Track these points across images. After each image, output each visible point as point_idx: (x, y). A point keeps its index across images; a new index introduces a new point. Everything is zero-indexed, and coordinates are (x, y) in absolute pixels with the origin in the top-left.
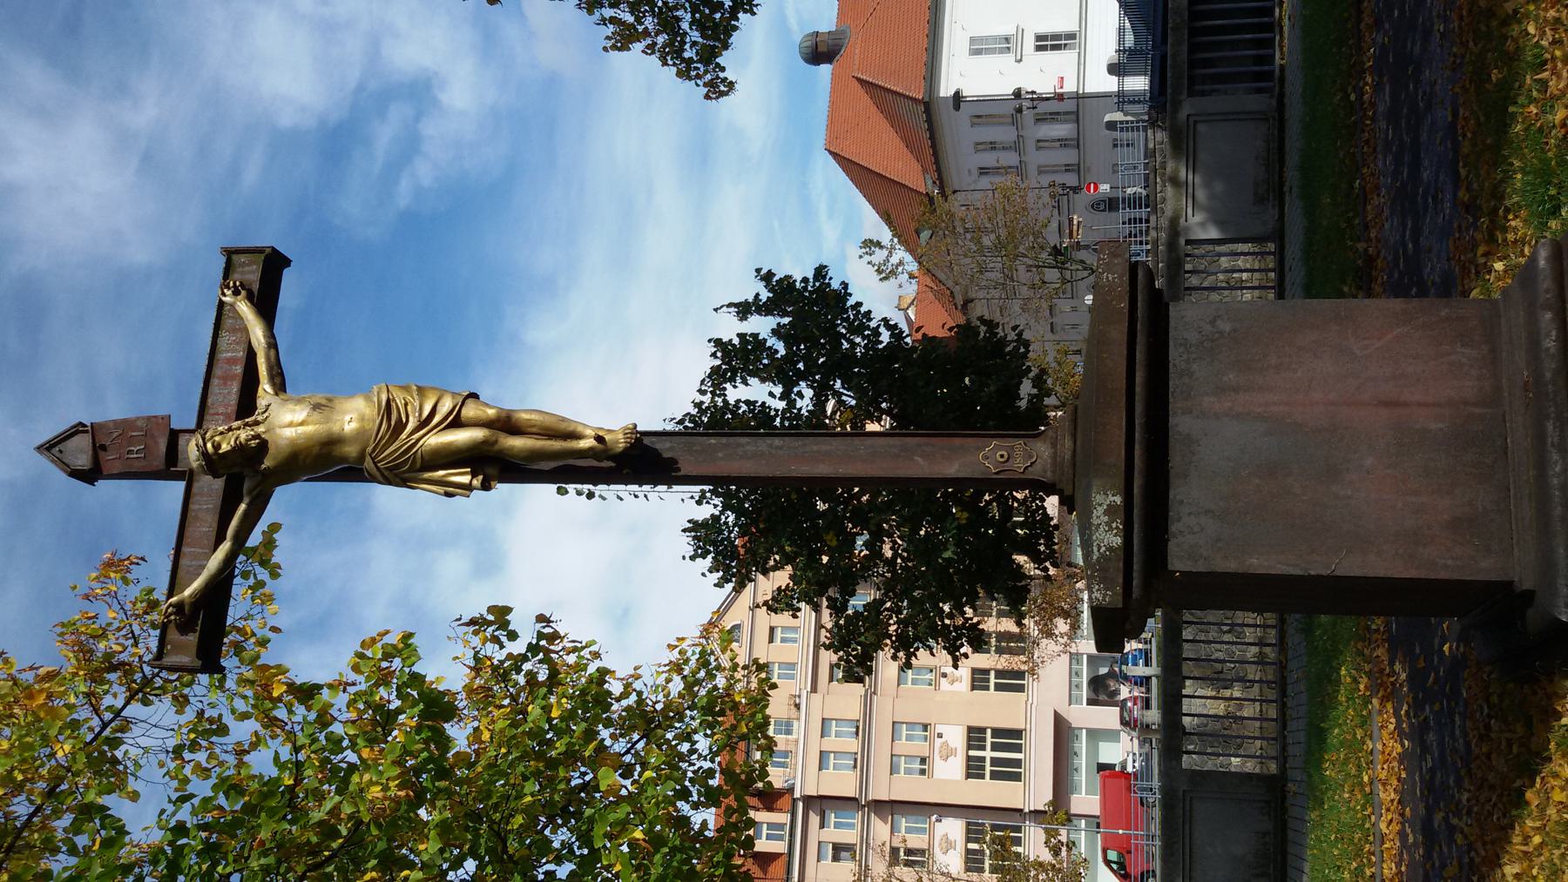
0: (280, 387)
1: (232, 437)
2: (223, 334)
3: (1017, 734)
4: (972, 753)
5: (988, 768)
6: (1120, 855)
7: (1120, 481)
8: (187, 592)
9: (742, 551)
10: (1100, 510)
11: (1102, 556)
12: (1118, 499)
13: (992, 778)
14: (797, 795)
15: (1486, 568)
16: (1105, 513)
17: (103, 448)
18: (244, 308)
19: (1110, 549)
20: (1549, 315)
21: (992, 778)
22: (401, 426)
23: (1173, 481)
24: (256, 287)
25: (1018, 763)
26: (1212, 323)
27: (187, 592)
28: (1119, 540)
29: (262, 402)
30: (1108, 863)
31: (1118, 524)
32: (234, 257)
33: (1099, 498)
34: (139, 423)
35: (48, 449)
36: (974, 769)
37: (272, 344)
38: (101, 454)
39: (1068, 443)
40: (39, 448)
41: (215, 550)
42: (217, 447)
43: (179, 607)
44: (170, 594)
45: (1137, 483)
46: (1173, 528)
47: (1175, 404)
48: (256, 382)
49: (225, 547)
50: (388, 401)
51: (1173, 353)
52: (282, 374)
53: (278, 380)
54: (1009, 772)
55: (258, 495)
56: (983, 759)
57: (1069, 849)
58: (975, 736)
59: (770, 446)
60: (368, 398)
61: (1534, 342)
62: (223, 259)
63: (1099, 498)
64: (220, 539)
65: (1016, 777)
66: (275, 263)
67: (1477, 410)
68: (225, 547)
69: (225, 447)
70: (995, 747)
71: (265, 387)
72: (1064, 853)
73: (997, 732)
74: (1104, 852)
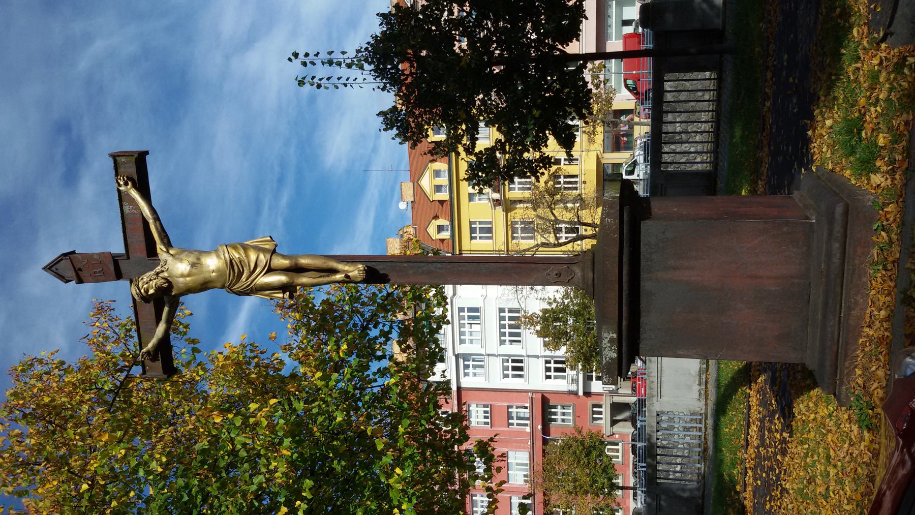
0: (168, 245)
1: (153, 283)
2: (125, 204)
6: (634, 82)
7: (616, 327)
8: (150, 345)
9: (413, 125)
10: (606, 340)
11: (607, 362)
12: (615, 336)
15: (792, 357)
16: (609, 342)
17: (80, 269)
18: (134, 194)
19: (611, 359)
20: (837, 245)
22: (241, 274)
23: (643, 314)
24: (135, 177)
26: (664, 233)
28: (615, 355)
30: (627, 86)
31: (615, 347)
32: (117, 158)
33: (605, 335)
34: (95, 257)
35: (50, 269)
37: (153, 211)
38: (79, 272)
39: (591, 274)
40: (44, 268)
41: (157, 325)
42: (147, 291)
43: (148, 353)
44: (141, 349)
45: (624, 323)
46: (642, 336)
47: (644, 275)
49: (162, 327)
50: (231, 260)
51: (643, 249)
52: (167, 236)
53: (165, 241)
57: (605, 84)
59: (436, 268)
60: (218, 257)
61: (829, 256)
62: (111, 161)
63: (605, 335)
64: (158, 320)
66: (141, 159)
67: (796, 281)
68: (162, 327)
69: (151, 291)
71: (160, 247)
72: (602, 85)
74: (625, 81)
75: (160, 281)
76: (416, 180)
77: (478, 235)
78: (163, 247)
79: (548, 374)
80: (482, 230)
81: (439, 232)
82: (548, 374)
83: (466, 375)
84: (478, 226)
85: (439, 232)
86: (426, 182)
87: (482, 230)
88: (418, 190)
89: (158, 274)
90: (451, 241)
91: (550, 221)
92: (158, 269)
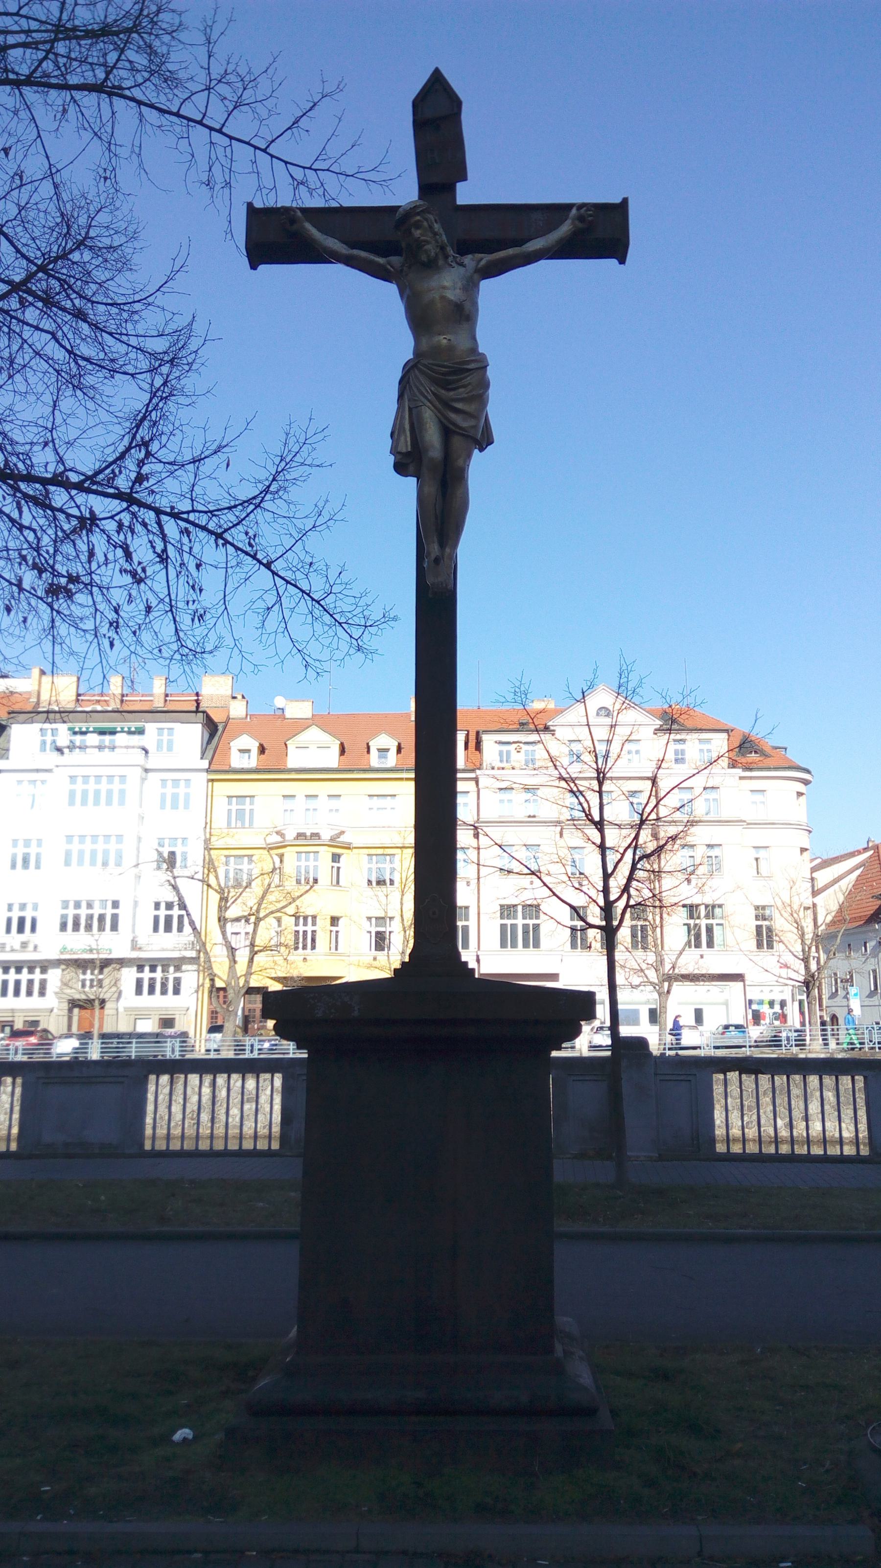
1: (428, 237)
3: (537, 945)
4: (520, 908)
5: (509, 922)
12: (356, 1014)
13: (501, 925)
14: (478, 772)
21: (501, 925)
25: (514, 945)
27: (308, 226)
28: (319, 1014)
29: (468, 260)
36: (507, 910)
40: (437, 71)
42: (418, 225)
48: (491, 252)
54: (507, 938)
55: (387, 270)
56: (515, 918)
58: (507, 910)
65: (503, 945)
70: (526, 927)
73: (536, 927)
75: (431, 249)
76: (317, 720)
77: (234, 807)
78: (483, 262)
79: (163, 906)
80: (240, 814)
81: (379, 750)
82: (163, 906)
83: (164, 781)
84: (247, 807)
85: (379, 750)
86: (314, 734)
87: (240, 814)
88: (300, 726)
89: (443, 248)
90: (227, 768)
91: (258, 911)
92: (450, 251)
